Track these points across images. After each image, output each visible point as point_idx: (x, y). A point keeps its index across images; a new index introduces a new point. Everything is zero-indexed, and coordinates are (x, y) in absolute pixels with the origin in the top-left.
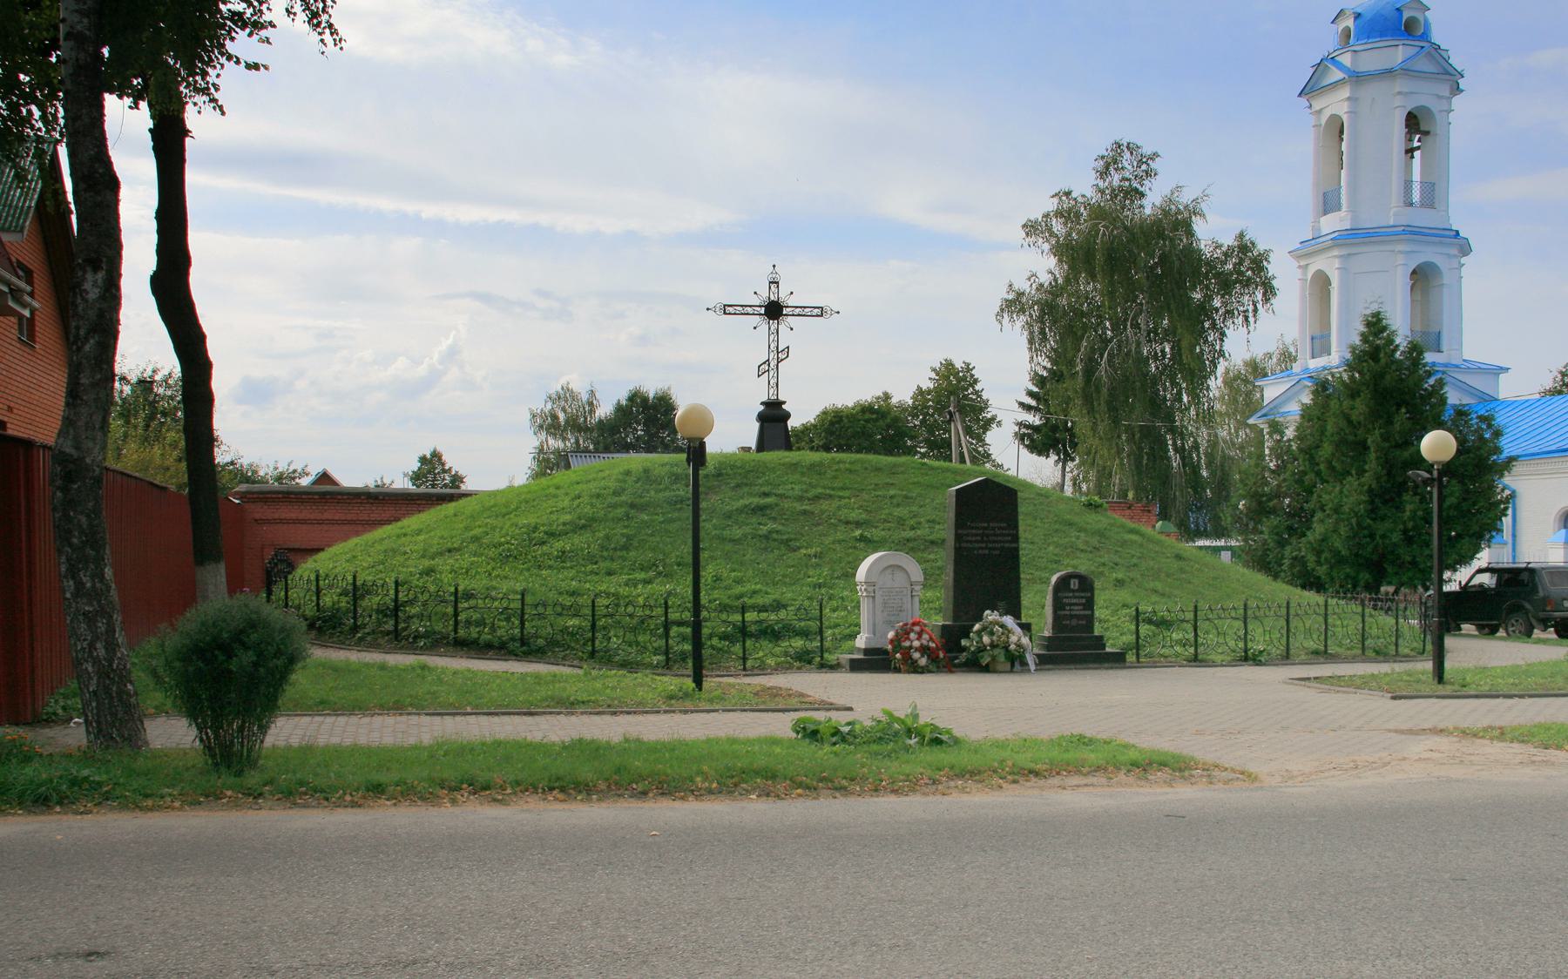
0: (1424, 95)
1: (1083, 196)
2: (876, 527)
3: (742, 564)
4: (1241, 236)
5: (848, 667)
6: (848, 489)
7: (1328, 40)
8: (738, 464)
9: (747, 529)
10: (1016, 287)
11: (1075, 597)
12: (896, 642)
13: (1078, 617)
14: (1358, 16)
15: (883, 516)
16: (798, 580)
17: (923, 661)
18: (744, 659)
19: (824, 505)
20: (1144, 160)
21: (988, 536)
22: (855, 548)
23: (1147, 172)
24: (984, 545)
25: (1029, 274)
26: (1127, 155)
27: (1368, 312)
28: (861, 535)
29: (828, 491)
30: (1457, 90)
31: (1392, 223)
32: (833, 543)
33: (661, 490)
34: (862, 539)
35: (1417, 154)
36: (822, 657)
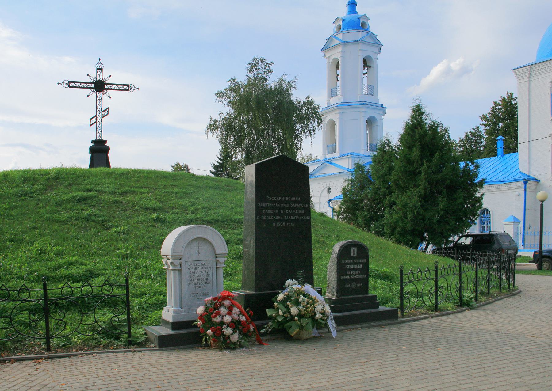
0: (369, 51)
1: (241, 82)
2: (168, 212)
3: (65, 240)
4: (308, 98)
5: (156, 343)
6: (146, 188)
7: (331, 29)
8: (72, 172)
9: (73, 214)
10: (214, 119)
11: (355, 263)
12: (207, 317)
13: (357, 281)
14: (343, 20)
15: (172, 205)
16: (110, 252)
17: (235, 337)
18: (48, 337)
19: (130, 197)
20: (268, 65)
21: (284, 208)
22: (153, 226)
23: (268, 70)
24: (281, 218)
25: (219, 113)
26: (260, 63)
27: (415, 104)
28: (158, 218)
29: (133, 189)
30: (380, 51)
31: (359, 101)
32: (137, 223)
33: (13, 187)
34: (158, 219)
36: (129, 333)
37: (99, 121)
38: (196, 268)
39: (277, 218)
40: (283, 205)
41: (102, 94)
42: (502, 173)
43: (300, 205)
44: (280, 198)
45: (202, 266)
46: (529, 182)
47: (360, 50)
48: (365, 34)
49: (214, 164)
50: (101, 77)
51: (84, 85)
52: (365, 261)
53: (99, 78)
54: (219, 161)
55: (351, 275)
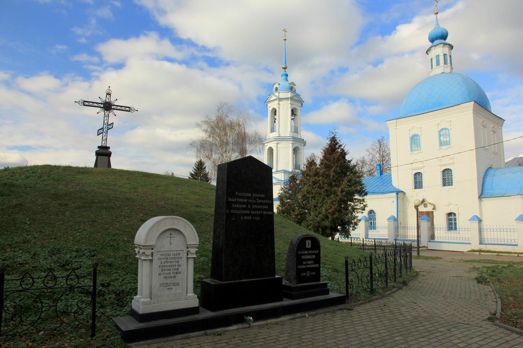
11: (310, 254)
13: (311, 270)
21: (251, 204)
24: (248, 212)
38: (167, 258)
39: (244, 212)
40: (250, 201)
41: (109, 112)
42: (381, 187)
43: (265, 201)
44: (248, 195)
45: (173, 257)
46: (399, 193)
49: (192, 173)
50: (109, 100)
51: (96, 105)
52: (317, 252)
53: (107, 101)
54: (194, 170)
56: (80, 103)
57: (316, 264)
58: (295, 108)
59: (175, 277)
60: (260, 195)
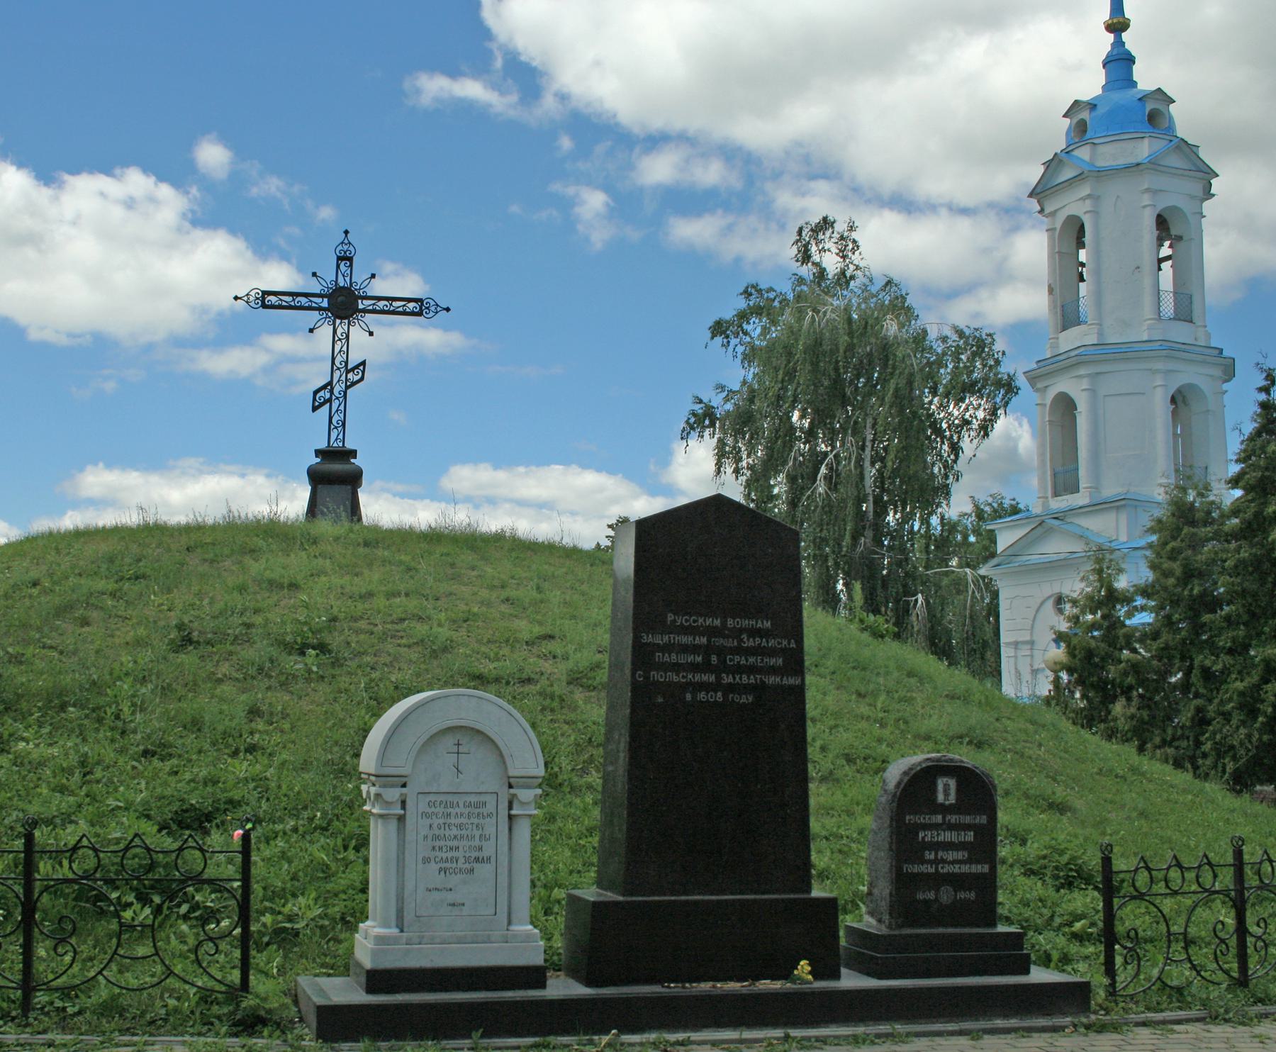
0: (1176, 194)
13: (958, 881)
21: (721, 652)
30: (1208, 195)
35: (1166, 266)
37: (337, 398)
40: (720, 641)
43: (772, 643)
45: (467, 810)
47: (1148, 190)
48: (1160, 145)
50: (348, 279)
51: (303, 300)
52: (982, 819)
55: (936, 862)
56: (252, 299)
57: (978, 862)
58: (1174, 209)
59: (472, 870)
60: (753, 622)
